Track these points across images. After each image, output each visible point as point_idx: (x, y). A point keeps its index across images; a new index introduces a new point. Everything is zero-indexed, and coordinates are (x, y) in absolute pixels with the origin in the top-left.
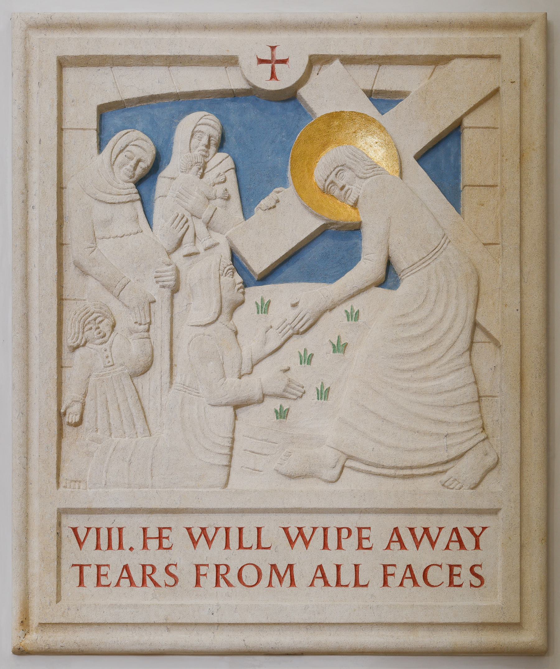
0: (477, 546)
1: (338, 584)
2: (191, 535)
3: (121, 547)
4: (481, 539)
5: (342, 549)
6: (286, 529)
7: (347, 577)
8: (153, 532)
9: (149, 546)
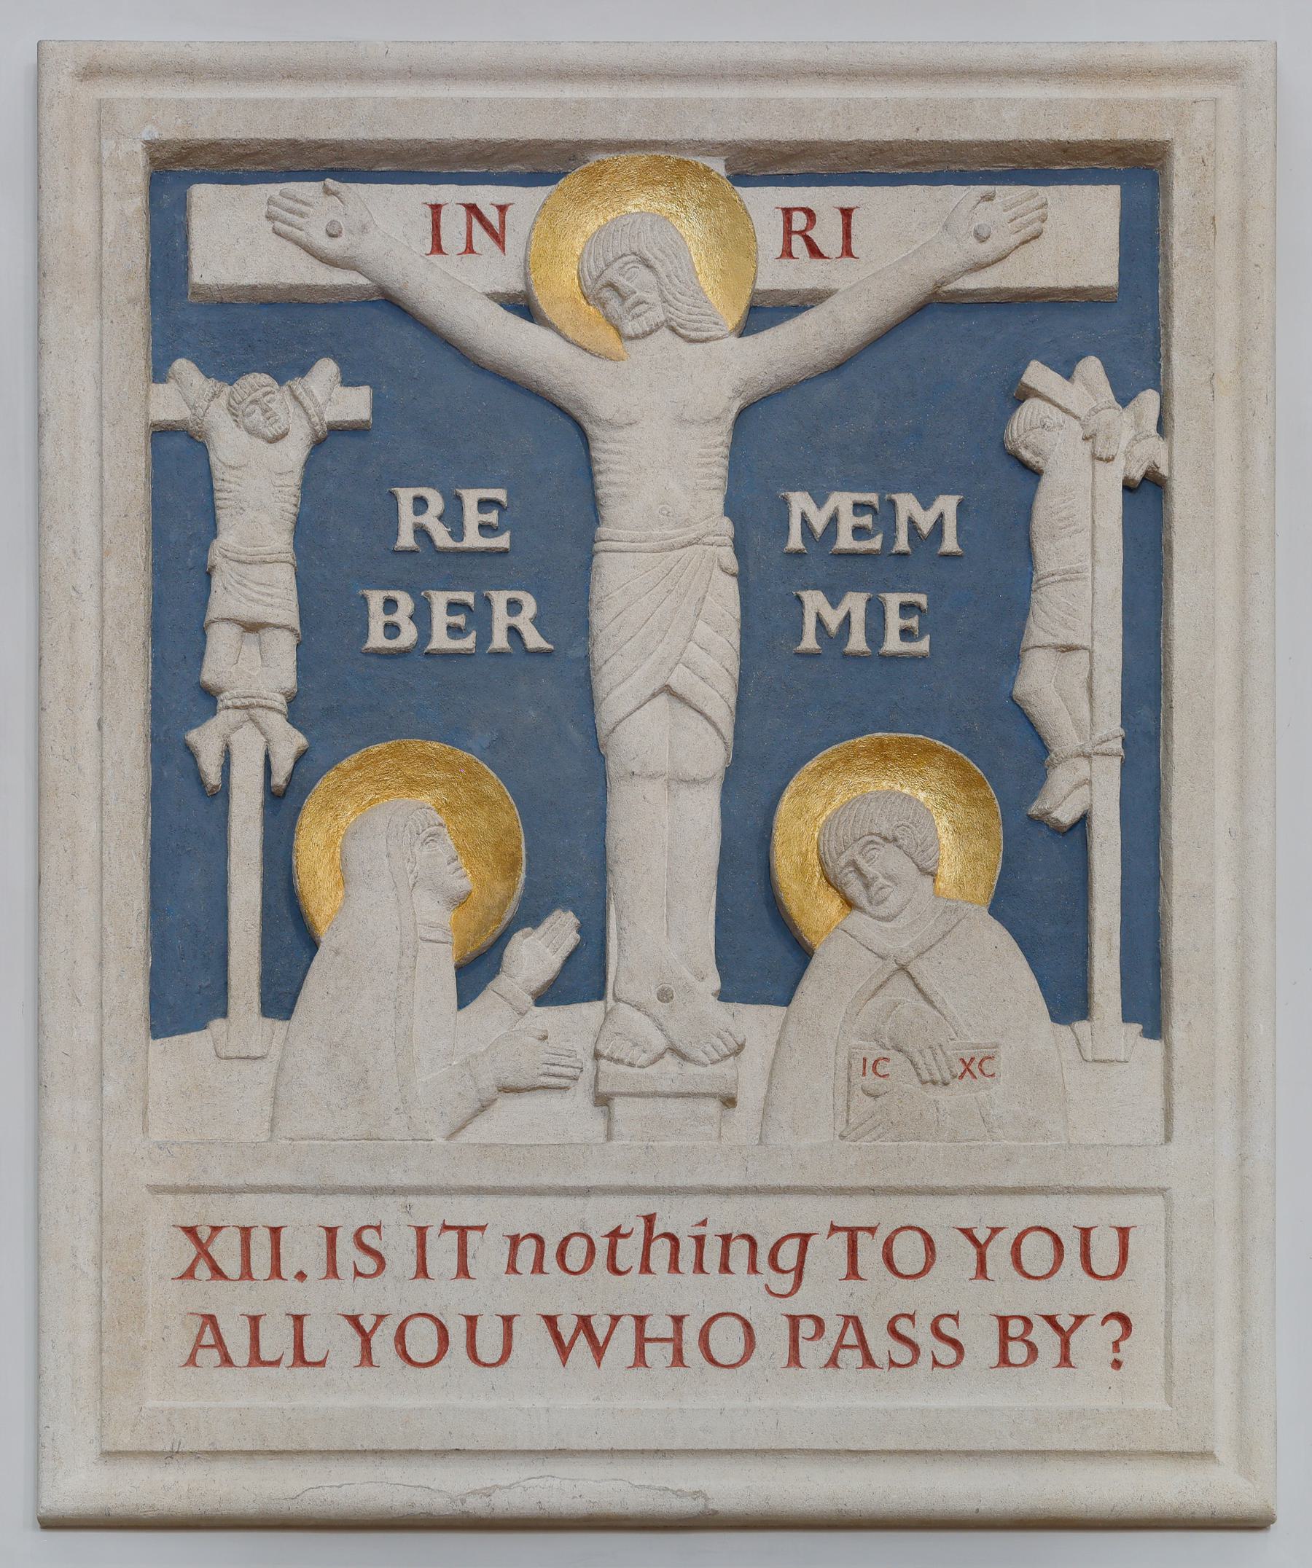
0: (1065, 1360)
1: (255, 1358)
2: (557, 1337)
3: (276, 1272)
4: (1074, 1339)
5: (465, 1316)
6: (551, 1321)
7: (276, 1341)
8: (659, 1326)
9: (670, 1323)
